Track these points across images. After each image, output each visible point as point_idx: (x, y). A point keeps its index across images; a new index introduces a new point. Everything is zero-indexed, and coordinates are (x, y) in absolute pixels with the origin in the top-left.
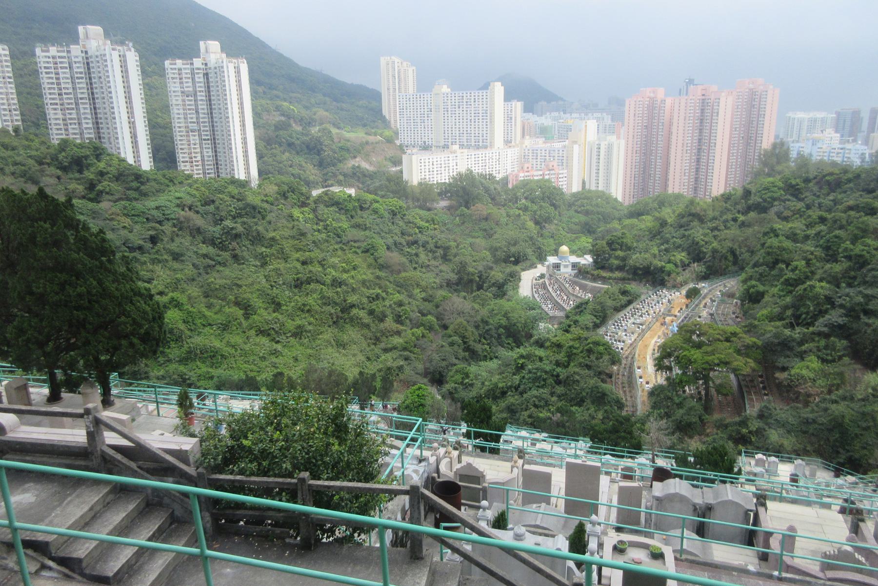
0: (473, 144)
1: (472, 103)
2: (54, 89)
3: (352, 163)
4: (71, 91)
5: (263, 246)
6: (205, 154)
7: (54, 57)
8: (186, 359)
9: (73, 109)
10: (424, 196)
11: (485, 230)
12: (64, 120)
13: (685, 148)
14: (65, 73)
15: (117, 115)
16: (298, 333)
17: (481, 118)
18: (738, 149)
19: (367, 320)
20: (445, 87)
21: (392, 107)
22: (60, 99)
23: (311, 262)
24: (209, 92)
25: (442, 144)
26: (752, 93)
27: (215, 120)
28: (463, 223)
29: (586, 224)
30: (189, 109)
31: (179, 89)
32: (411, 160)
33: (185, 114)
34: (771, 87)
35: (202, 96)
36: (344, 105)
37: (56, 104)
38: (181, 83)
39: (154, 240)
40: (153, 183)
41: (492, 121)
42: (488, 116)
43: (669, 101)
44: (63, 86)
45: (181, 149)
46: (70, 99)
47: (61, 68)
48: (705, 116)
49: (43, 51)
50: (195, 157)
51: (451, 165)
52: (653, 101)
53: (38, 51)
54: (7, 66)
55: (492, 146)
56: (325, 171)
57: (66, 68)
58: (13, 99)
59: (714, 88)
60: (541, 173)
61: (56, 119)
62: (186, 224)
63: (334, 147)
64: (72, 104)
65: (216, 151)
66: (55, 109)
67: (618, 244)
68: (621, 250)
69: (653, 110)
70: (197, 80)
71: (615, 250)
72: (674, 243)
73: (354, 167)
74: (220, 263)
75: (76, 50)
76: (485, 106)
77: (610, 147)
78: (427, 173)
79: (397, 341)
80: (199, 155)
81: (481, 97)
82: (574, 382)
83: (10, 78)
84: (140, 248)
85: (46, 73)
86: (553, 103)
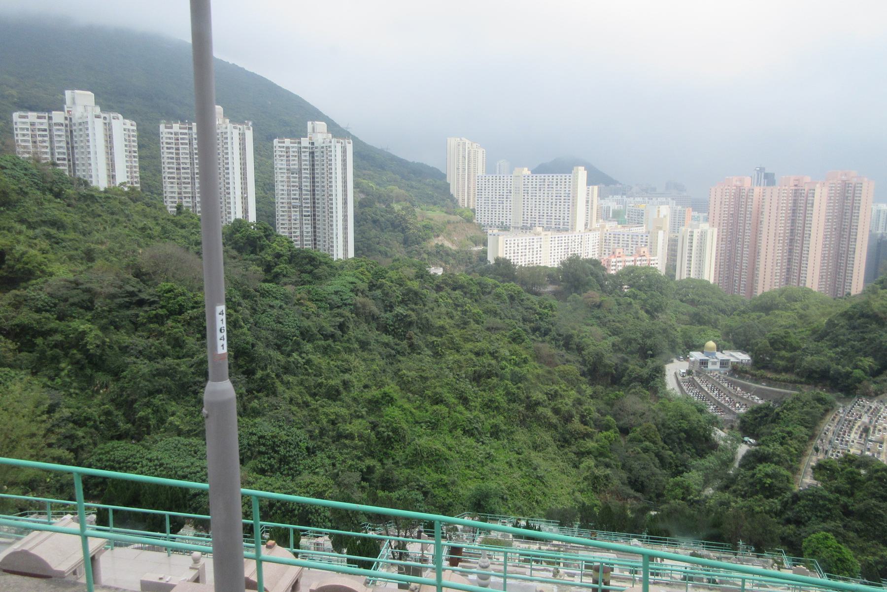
0: (553, 226)
1: (554, 186)
2: (173, 163)
3: (434, 242)
4: (188, 166)
5: (431, 334)
6: (305, 230)
7: (176, 134)
8: (412, 462)
9: (188, 183)
10: (532, 279)
11: (599, 318)
12: (179, 193)
13: (778, 238)
14: (184, 148)
15: (231, 191)
16: (495, 433)
17: (562, 201)
18: (831, 241)
19: (554, 420)
20: (526, 169)
21: (461, 189)
22: (178, 174)
23: (483, 354)
24: (313, 170)
25: (521, 225)
26: (846, 185)
27: (317, 197)
28: (575, 310)
29: (696, 314)
30: (293, 186)
31: (285, 166)
32: (497, 241)
33: (289, 190)
34: (866, 179)
35: (306, 174)
36: (414, 183)
37: (174, 178)
38: (288, 161)
39: (342, 327)
40: (325, 267)
41: (574, 205)
42: (571, 199)
43: (757, 190)
44: (182, 161)
45: (282, 224)
46: (187, 173)
47: (182, 144)
48: (798, 208)
49: (166, 128)
50: (295, 232)
51: (535, 247)
52: (740, 189)
53: (162, 128)
54: (134, 141)
55: (573, 229)
56: (410, 249)
57: (186, 144)
58: (135, 172)
59: (808, 179)
60: (633, 258)
61: (172, 192)
62: (361, 310)
63: (419, 225)
64: (188, 178)
65: (315, 227)
66: (172, 183)
67: (781, 343)
68: (784, 349)
69: (740, 198)
70: (303, 158)
71: (779, 349)
72: (853, 347)
73: (437, 246)
74: (398, 352)
75: (58, 116)
76: (567, 189)
77: (703, 235)
78: (512, 255)
79: (591, 444)
80: (298, 230)
81: (563, 181)
82: (876, 516)
83: (135, 152)
84: (332, 336)
85: (168, 148)
86: (612, 186)
